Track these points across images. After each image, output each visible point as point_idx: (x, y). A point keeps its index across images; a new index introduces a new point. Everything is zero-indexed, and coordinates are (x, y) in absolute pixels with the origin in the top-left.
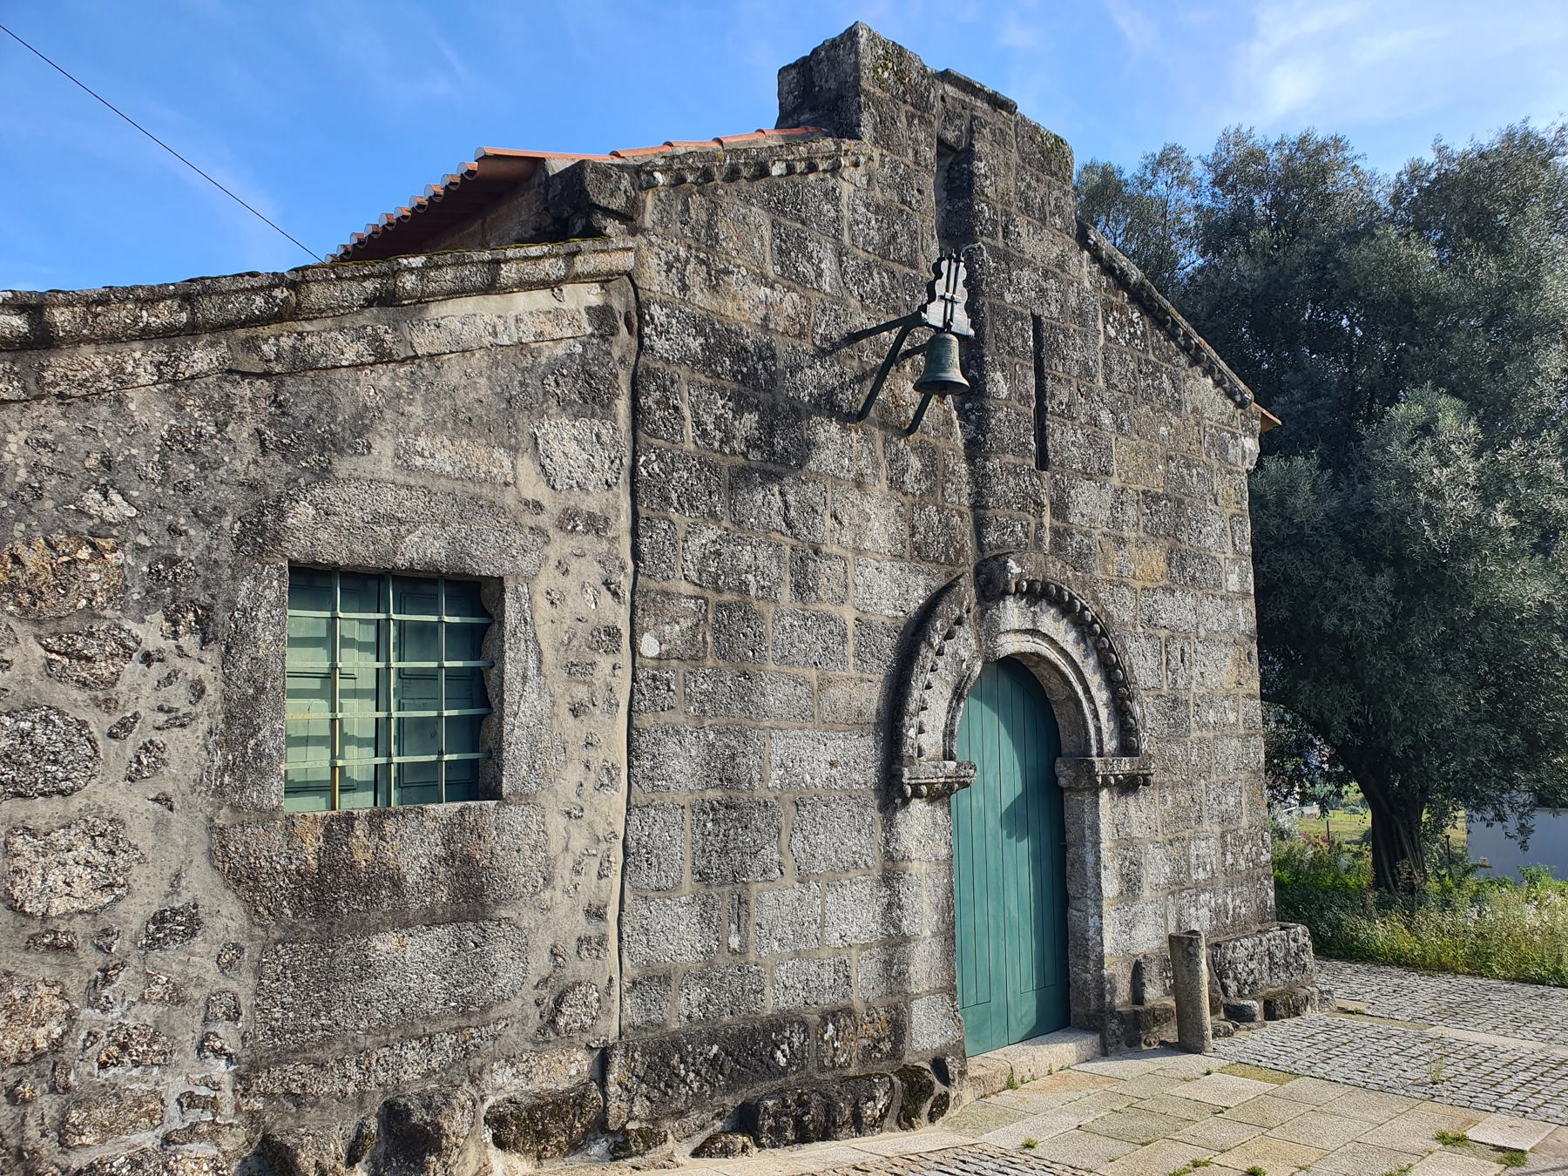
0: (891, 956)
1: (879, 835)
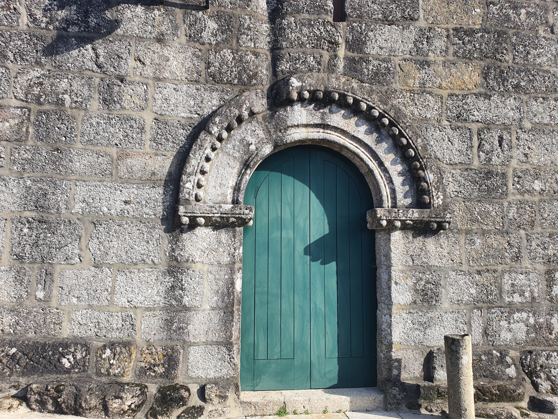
1: (166, 245)
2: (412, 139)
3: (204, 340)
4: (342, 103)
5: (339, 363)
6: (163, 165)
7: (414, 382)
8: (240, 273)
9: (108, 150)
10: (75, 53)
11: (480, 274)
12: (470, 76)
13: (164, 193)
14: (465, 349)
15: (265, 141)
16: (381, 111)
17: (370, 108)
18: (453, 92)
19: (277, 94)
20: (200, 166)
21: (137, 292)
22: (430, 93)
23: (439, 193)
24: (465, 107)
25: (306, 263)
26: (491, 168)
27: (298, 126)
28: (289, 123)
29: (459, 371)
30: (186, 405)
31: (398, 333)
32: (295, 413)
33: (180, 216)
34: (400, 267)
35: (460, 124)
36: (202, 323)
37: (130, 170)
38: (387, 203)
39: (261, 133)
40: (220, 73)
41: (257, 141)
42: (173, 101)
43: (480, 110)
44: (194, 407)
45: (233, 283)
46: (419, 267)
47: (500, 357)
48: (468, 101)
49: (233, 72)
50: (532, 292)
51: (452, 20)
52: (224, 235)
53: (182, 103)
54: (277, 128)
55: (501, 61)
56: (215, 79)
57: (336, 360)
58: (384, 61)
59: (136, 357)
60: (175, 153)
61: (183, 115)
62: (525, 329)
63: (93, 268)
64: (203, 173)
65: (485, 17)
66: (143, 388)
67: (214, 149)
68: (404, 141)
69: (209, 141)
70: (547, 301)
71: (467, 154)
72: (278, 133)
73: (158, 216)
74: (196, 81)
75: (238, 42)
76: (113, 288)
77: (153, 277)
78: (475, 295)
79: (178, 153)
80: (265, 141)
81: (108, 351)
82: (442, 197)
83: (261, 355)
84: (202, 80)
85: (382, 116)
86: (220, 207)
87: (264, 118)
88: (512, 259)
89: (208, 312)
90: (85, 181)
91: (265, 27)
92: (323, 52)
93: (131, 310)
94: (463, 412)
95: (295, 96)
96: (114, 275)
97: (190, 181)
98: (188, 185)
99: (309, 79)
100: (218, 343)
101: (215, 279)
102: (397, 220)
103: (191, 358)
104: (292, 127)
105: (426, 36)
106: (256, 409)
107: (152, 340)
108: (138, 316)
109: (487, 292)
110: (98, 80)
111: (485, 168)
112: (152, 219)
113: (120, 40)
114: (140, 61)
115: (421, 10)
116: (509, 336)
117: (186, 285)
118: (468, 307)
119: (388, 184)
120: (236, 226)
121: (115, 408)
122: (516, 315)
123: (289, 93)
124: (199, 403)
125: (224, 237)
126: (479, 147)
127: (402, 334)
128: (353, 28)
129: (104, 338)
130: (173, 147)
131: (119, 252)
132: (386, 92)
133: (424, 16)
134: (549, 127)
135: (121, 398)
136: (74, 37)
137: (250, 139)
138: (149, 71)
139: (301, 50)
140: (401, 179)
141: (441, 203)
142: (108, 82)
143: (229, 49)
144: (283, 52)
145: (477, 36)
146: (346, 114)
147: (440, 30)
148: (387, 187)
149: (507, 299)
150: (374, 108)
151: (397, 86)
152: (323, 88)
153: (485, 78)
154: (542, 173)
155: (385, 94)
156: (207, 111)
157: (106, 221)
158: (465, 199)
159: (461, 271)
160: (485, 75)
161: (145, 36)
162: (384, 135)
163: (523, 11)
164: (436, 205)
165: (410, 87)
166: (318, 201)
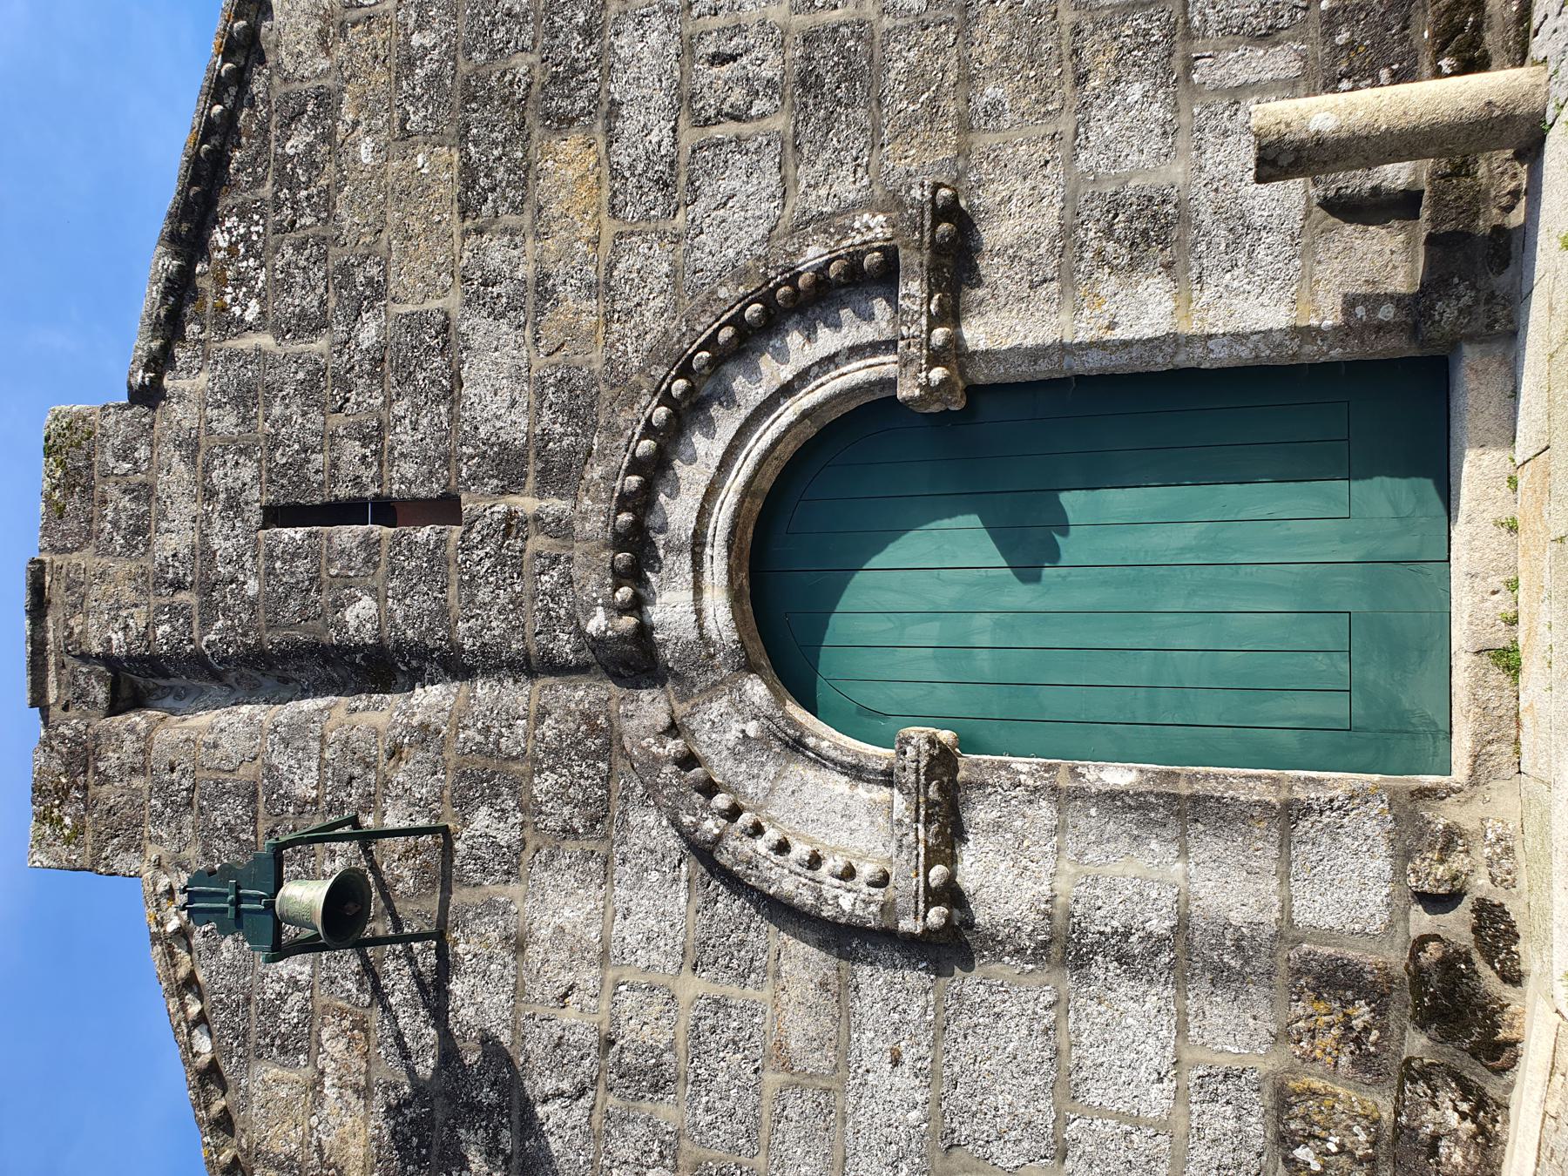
0: (1209, 966)
1: (1009, 967)
2: (719, 312)
3: (1275, 883)
4: (641, 503)
5: (1367, 474)
6: (802, 961)
7: (1421, 249)
8: (1084, 771)
9: (769, 1092)
10: (555, 1145)
11: (1086, 75)
12: (567, 161)
13: (871, 964)
14: (1288, 125)
15: (736, 694)
16: (655, 402)
17: (649, 430)
18: (606, 206)
19: (626, 665)
20: (799, 869)
21: (1133, 1055)
22: (611, 267)
23: (857, 225)
24: (640, 168)
25: (1064, 577)
26: (793, 78)
27: (699, 612)
28: (693, 635)
29: (1360, 137)
30: (1468, 953)
31: (1261, 311)
32: (1513, 622)
33: (926, 930)
34: (1065, 317)
35: (683, 179)
36: (1227, 886)
37: (815, 1045)
38: (885, 365)
39: (719, 706)
40: (585, 803)
41: (736, 717)
42: (651, 922)
43: (648, 128)
44: (1475, 930)
45: (1113, 795)
46: (1066, 260)
48: (626, 161)
49: (581, 773)
51: (444, 224)
52: (979, 814)
53: (655, 905)
54: (706, 664)
55: (529, 85)
56: (599, 817)
57: (1354, 484)
58: (541, 395)
59: (1321, 1077)
60: (773, 928)
61: (682, 900)
63: (1068, 1163)
64: (815, 861)
65: (435, 139)
66: (1411, 1072)
67: (757, 830)
68: (727, 333)
69: (738, 843)
71: (756, 152)
72: (716, 662)
73: (929, 985)
74: (606, 863)
75: (517, 758)
76: (1119, 1116)
77: (1093, 1008)
78: (1147, 84)
79: (771, 919)
80: (736, 694)
81: (1301, 1153)
82: (866, 216)
83: (1337, 708)
84: (602, 849)
85: (667, 398)
86: (900, 823)
87: (683, 698)
89: (1192, 866)
90: (846, 1159)
91: (483, 689)
92: (528, 551)
93: (1184, 1077)
94: (1497, 112)
95: (628, 622)
96: (1087, 1111)
97: (836, 897)
98: (847, 902)
99: (589, 587)
100: (1285, 843)
101: (1101, 843)
102: (929, 339)
103: (1329, 921)
104: (701, 627)
105: (480, 288)
106: (1499, 740)
107: (1273, 1028)
108: (1201, 1059)
109: (1138, 48)
110: (612, 1100)
111: (793, 94)
112: (938, 1000)
113: (524, 1037)
114: (566, 995)
115: (426, 306)
117: (1115, 923)
118: (1183, 103)
119: (837, 367)
120: (953, 781)
121: (1465, 1158)
123: (622, 638)
124: (1464, 910)
125: (982, 815)
126: (737, 119)
127: (1265, 299)
128: (473, 477)
129: (1264, 1158)
130: (757, 929)
131: (1024, 1091)
132: (613, 386)
133: (439, 297)
135: (1436, 1138)
136: (522, 1141)
137: (732, 736)
138: (588, 977)
139: (527, 605)
140: (823, 333)
141: (881, 218)
142: (614, 1076)
143: (531, 780)
144: (534, 649)
145: (475, 156)
146: (668, 490)
147: (467, 254)
148: (844, 370)
150: (649, 420)
151: (597, 359)
152: (608, 554)
153: (571, 121)
155: (617, 390)
156: (673, 842)
157: (943, 1117)
158: (875, 144)
159: (1076, 135)
160: (564, 122)
161: (512, 981)
162: (715, 388)
163: (416, 40)
164: (889, 233)
165: (597, 323)
166: (891, 548)
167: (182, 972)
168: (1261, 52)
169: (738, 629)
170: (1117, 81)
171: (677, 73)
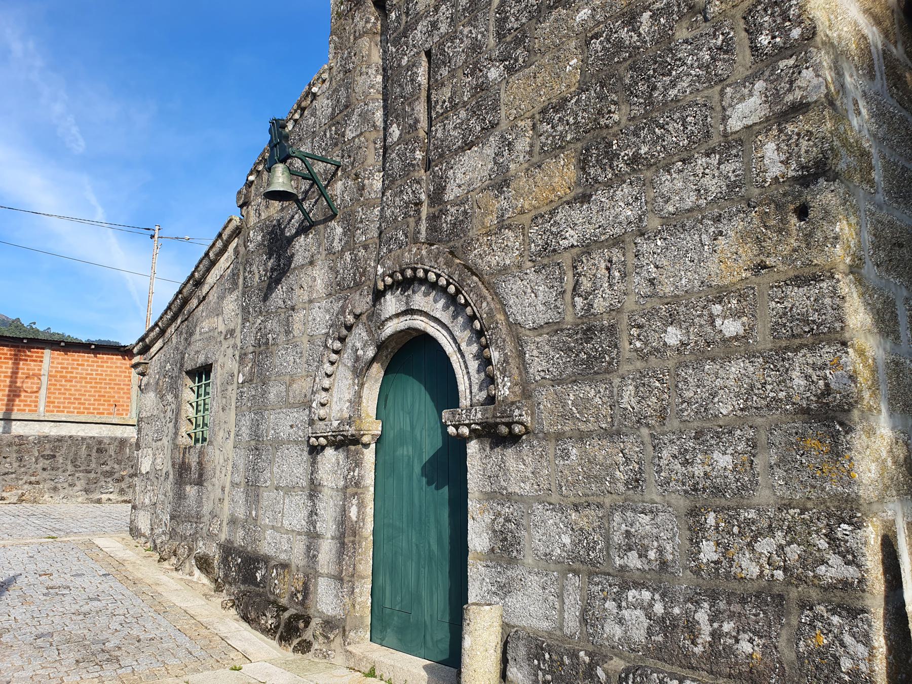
24: (554, 229)
27: (390, 318)
31: (474, 595)
43: (575, 227)
47: (589, 664)
50: (661, 551)
62: (646, 623)
70: (688, 572)
88: (627, 484)
116: (618, 631)
118: (559, 566)
122: (632, 594)
126: (574, 289)
134: (695, 213)
149: (618, 562)
153: (583, 169)
154: (682, 309)
159: (550, 504)
167: (303, 104)
168: (578, 614)
169: (387, 339)
170: (572, 529)
171: (603, 238)
